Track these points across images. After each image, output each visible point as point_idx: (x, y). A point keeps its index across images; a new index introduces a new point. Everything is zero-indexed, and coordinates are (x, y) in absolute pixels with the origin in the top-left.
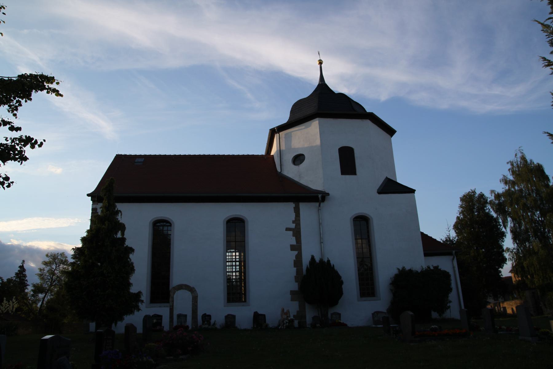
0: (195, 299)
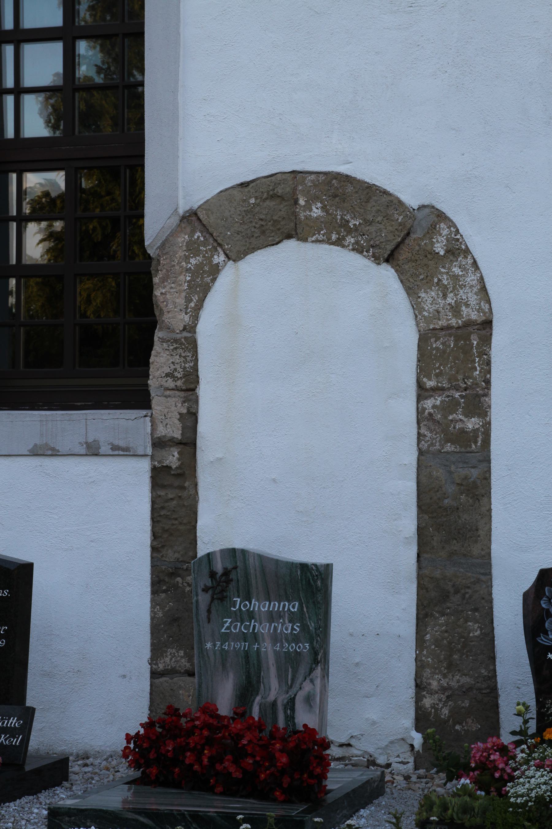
0: (455, 364)
